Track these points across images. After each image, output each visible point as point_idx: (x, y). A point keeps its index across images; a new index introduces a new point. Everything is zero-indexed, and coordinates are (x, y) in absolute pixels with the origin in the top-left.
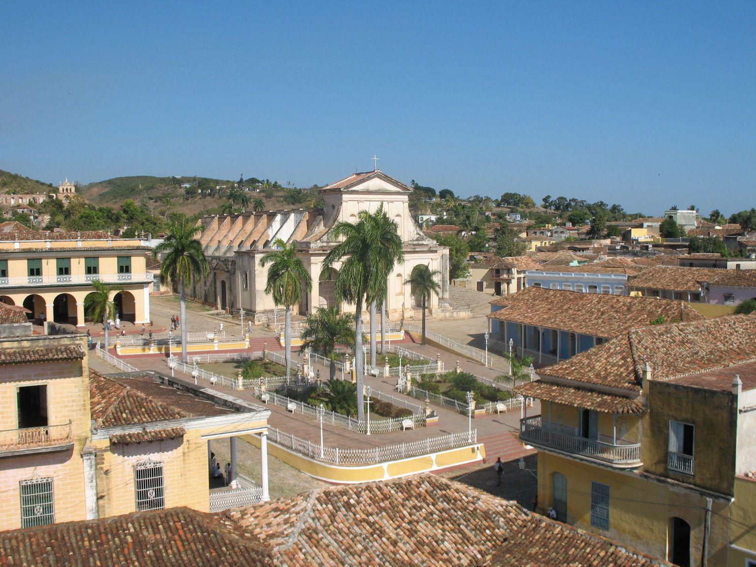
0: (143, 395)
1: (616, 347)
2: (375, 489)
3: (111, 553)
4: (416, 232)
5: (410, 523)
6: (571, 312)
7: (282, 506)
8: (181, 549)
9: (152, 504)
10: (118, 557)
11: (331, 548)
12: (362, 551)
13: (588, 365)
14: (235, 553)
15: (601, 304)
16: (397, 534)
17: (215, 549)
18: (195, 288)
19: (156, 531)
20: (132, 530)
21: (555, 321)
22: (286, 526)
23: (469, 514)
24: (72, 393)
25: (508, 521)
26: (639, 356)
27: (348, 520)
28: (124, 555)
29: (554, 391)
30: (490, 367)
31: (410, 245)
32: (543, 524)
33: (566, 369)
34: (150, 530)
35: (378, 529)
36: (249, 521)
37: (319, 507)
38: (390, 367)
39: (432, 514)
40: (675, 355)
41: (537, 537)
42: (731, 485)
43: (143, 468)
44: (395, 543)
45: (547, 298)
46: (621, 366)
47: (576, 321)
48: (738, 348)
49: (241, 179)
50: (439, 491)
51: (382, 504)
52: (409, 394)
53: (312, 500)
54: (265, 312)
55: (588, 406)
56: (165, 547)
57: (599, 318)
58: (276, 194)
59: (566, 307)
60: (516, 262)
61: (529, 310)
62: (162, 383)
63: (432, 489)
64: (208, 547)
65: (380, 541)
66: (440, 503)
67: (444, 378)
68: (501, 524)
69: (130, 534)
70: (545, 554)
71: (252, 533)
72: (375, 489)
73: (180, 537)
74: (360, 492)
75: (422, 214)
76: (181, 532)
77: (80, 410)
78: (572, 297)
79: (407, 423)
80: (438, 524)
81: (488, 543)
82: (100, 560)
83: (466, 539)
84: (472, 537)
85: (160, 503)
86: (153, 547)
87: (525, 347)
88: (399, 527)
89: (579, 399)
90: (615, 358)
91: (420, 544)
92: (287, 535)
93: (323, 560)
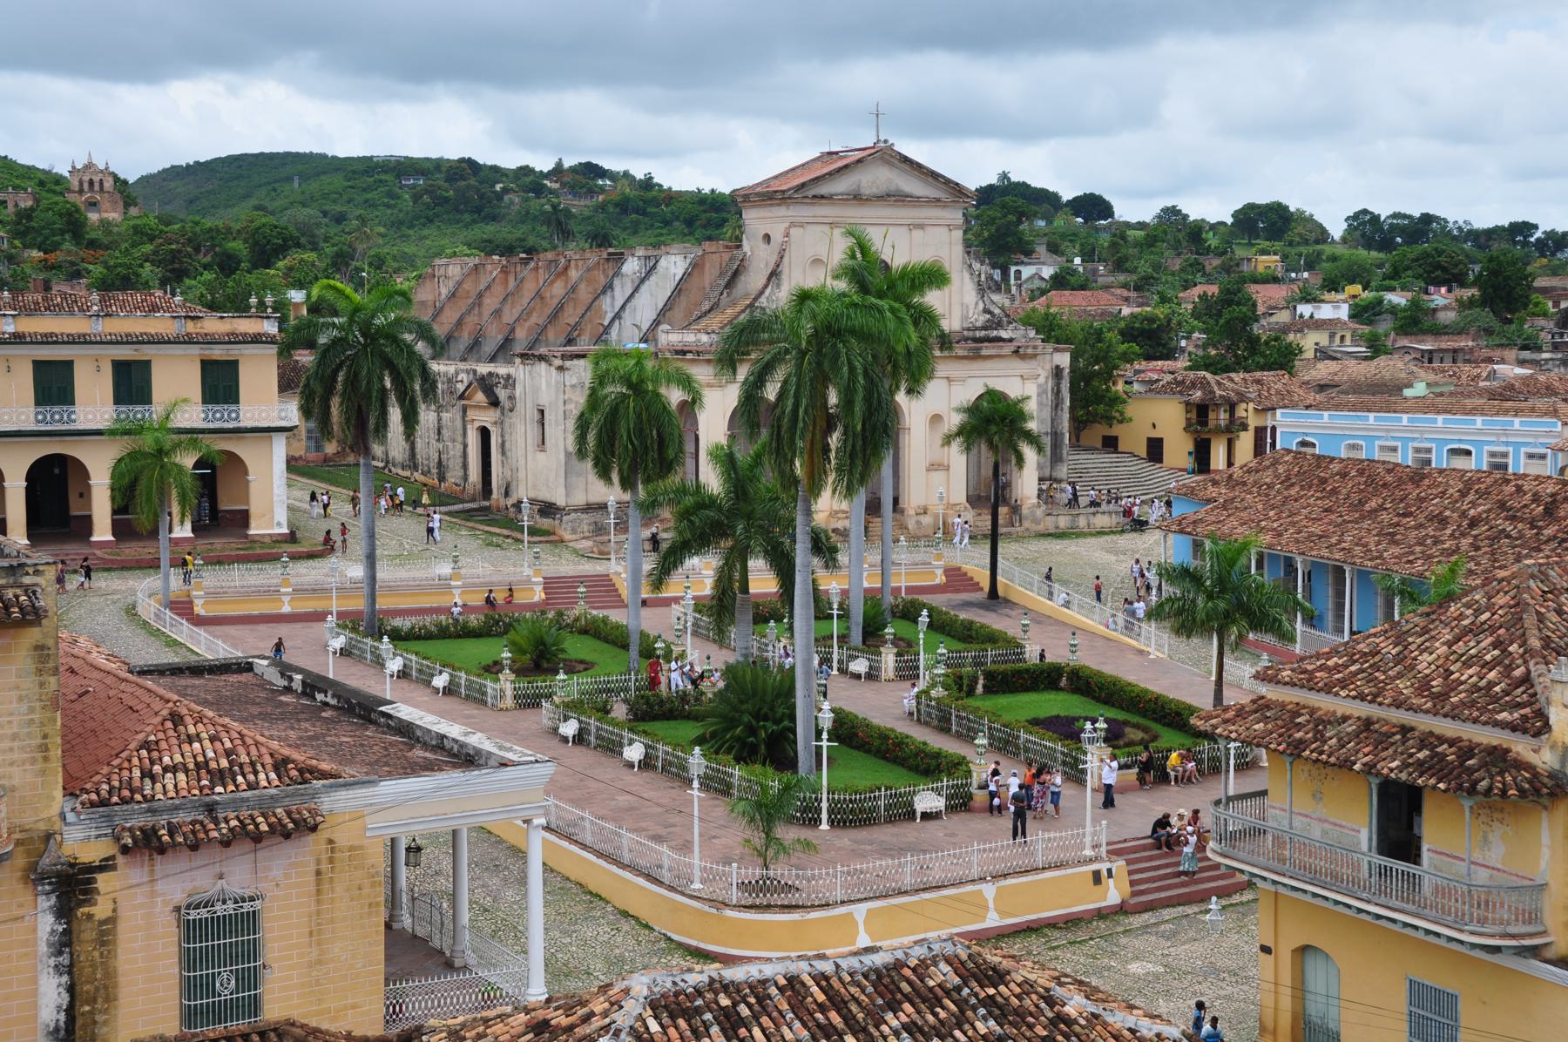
1: (1478, 612)
4: (981, 306)
6: (1384, 516)
9: (220, 1012)
15: (1471, 497)
21: (1339, 542)
24: (11, 714)
31: (966, 339)
38: (898, 654)
43: (204, 913)
45: (1323, 481)
46: (1490, 666)
47: (1397, 543)
55: (1392, 770)
57: (1463, 535)
59: (1373, 504)
61: (1272, 513)
63: (957, 980)
75: (1017, 264)
77: (33, 761)
78: (1389, 479)
85: (255, 1006)
89: (1366, 750)
90: (1472, 644)
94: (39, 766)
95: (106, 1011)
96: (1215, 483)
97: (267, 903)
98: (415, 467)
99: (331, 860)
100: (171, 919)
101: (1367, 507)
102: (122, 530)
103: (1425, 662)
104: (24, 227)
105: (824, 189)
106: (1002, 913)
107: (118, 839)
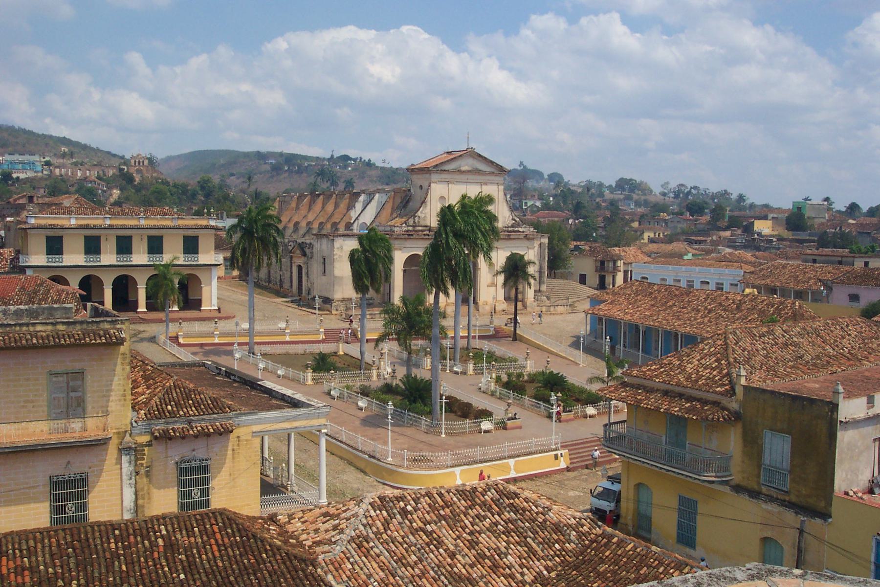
2: (436, 495)
3: (139, 557)
5: (471, 533)
7: (332, 511)
8: (217, 554)
10: (146, 562)
11: (382, 558)
12: (416, 563)
13: (680, 366)
14: (277, 560)
16: (456, 546)
17: (254, 556)
18: (269, 272)
19: (190, 533)
20: (164, 532)
22: (334, 533)
23: (538, 526)
25: (580, 535)
26: (735, 359)
27: (402, 528)
28: (154, 559)
29: (639, 394)
30: (583, 370)
32: (615, 540)
33: (655, 370)
34: (184, 532)
35: (435, 539)
36: (296, 526)
37: (373, 513)
39: (496, 524)
40: (776, 358)
41: (607, 554)
42: (829, 504)
43: (187, 465)
44: (452, 556)
45: (651, 293)
46: (713, 369)
47: (680, 320)
48: (849, 353)
49: (332, 156)
50: (506, 500)
51: (442, 512)
52: (493, 394)
53: (364, 506)
54: (343, 300)
56: (199, 552)
57: (706, 316)
58: (369, 173)
60: (622, 254)
62: (219, 374)
64: (247, 553)
65: (436, 553)
66: (506, 513)
67: (533, 378)
68: (572, 537)
69: (162, 536)
70: (614, 573)
71: (297, 539)
72: (436, 495)
73: (216, 541)
74: (419, 498)
76: (218, 536)
77: (120, 400)
78: (677, 293)
79: (486, 425)
80: (503, 536)
81: (556, 558)
82: (126, 565)
83: (532, 552)
84: (540, 552)
85: (207, 503)
86: (186, 551)
87: (625, 346)
88: (459, 537)
91: (481, 556)
92: (335, 543)
93: (372, 571)
94: (122, 403)
95: (149, 503)
96: (607, 294)
97: (213, 462)
98: (269, 282)
99: (238, 445)
100: (175, 466)
101: (668, 305)
102: (150, 307)
103: (689, 368)
105: (446, 167)
106: (517, 472)
107: (153, 434)
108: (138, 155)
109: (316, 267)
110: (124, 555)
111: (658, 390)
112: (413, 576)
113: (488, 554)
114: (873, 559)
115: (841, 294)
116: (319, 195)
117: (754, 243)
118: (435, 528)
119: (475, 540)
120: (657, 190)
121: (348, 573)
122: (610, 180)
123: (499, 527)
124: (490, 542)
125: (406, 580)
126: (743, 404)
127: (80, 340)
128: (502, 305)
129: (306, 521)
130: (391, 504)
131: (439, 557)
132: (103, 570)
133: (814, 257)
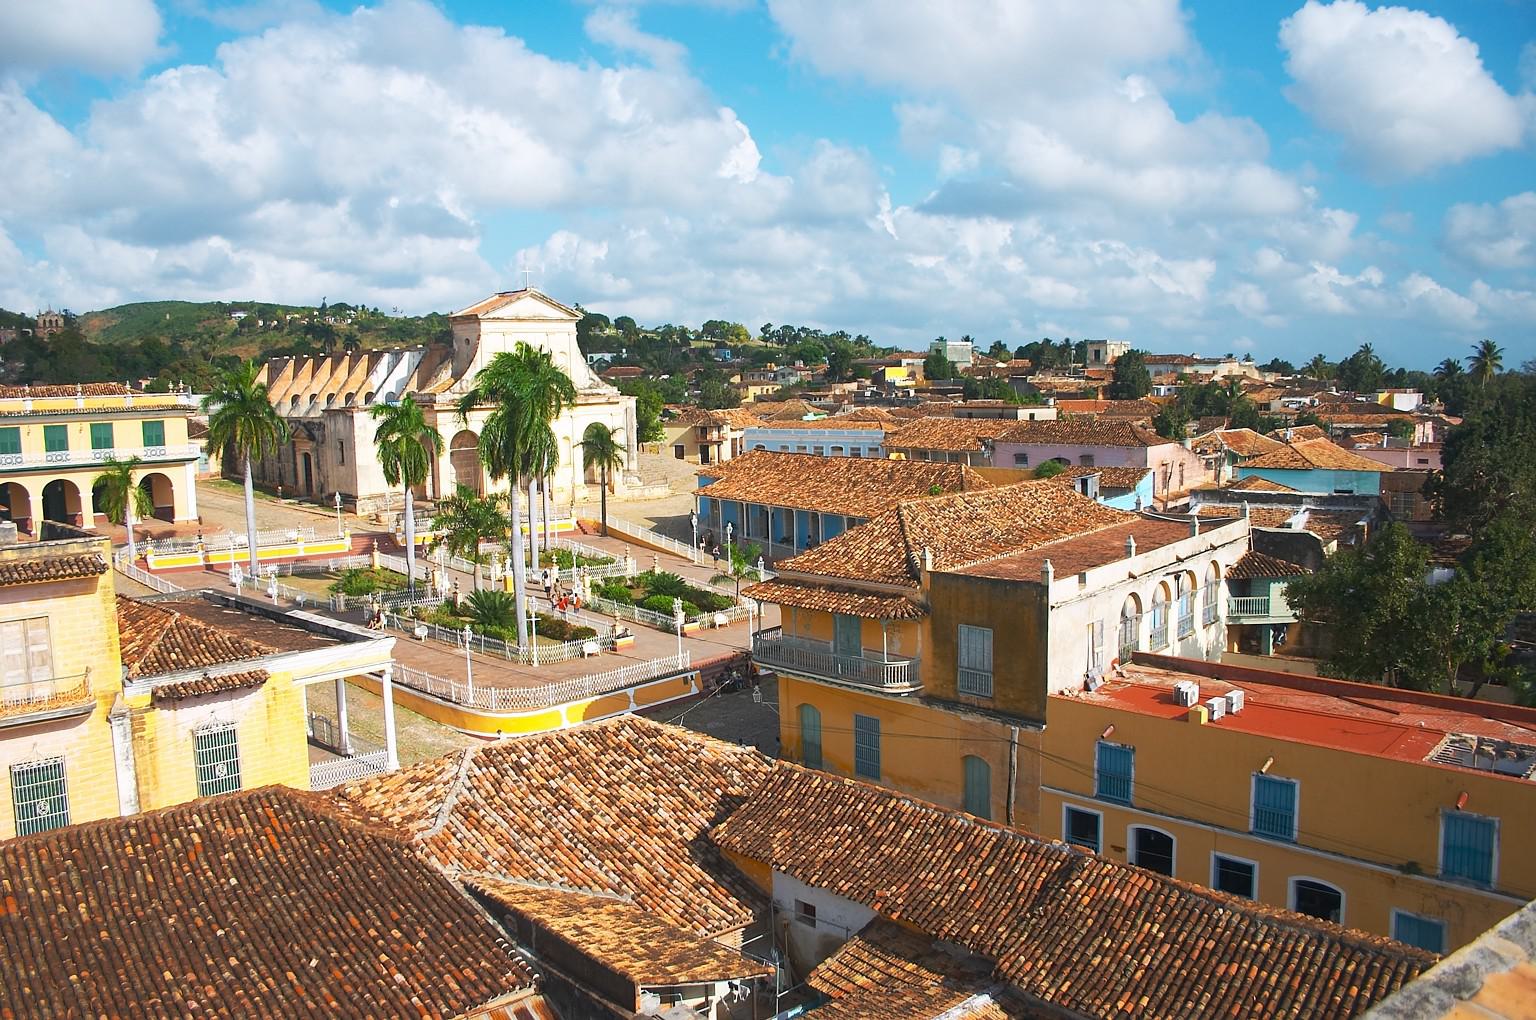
0: (201, 625)
1: (882, 527)
2: (555, 741)
5: (608, 786)
7: (421, 774)
8: (278, 847)
9: (219, 786)
11: (498, 828)
13: (845, 554)
17: (329, 844)
20: (199, 825)
25: (745, 775)
26: (914, 539)
27: (519, 787)
29: (798, 592)
32: (797, 775)
33: (814, 560)
36: (374, 799)
37: (478, 772)
43: (206, 733)
44: (589, 816)
45: (777, 465)
48: (1043, 524)
49: (324, 305)
50: (646, 739)
51: (567, 762)
53: (467, 763)
56: (252, 847)
60: (728, 417)
66: (648, 756)
67: (637, 582)
69: (197, 831)
71: (380, 816)
72: (555, 741)
74: (534, 747)
77: (104, 652)
79: (590, 646)
80: (648, 785)
85: (238, 782)
86: (233, 847)
91: (625, 814)
93: (488, 847)
99: (274, 699)
104: (9, 351)
108: (48, 313)
109: (330, 455)
110: (148, 861)
111: (820, 586)
112: (542, 848)
113: (634, 810)
114: (1096, 766)
115: (1005, 453)
116: (324, 358)
117: (885, 394)
118: (561, 783)
119: (615, 793)
120: (755, 334)
121: (457, 852)
122: (694, 324)
123: (642, 774)
124: (635, 795)
125: (534, 854)
126: (930, 595)
127: (42, 572)
128: (584, 491)
129: (387, 791)
130: (500, 758)
131: (572, 820)
132: (121, 885)
133: (969, 411)
